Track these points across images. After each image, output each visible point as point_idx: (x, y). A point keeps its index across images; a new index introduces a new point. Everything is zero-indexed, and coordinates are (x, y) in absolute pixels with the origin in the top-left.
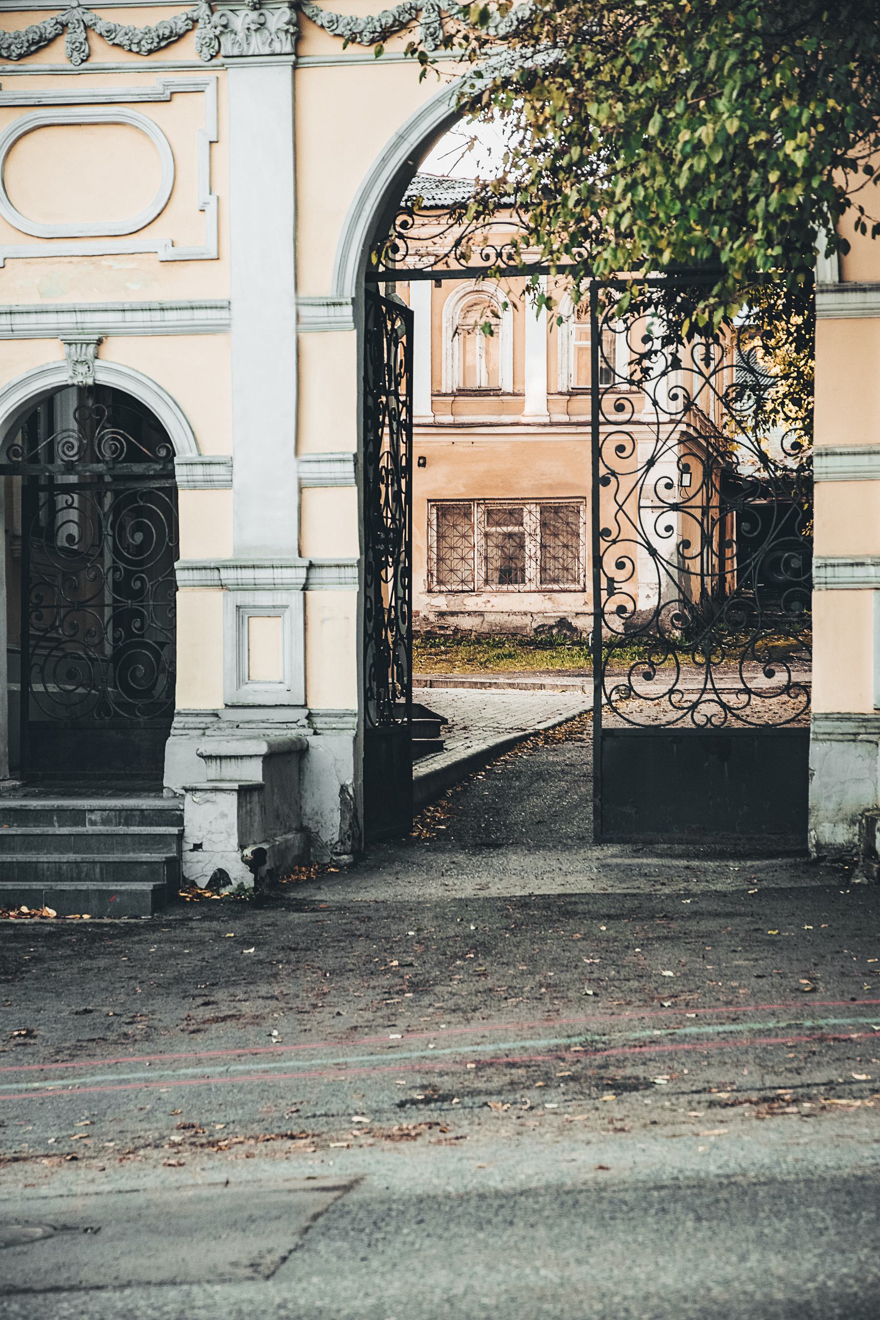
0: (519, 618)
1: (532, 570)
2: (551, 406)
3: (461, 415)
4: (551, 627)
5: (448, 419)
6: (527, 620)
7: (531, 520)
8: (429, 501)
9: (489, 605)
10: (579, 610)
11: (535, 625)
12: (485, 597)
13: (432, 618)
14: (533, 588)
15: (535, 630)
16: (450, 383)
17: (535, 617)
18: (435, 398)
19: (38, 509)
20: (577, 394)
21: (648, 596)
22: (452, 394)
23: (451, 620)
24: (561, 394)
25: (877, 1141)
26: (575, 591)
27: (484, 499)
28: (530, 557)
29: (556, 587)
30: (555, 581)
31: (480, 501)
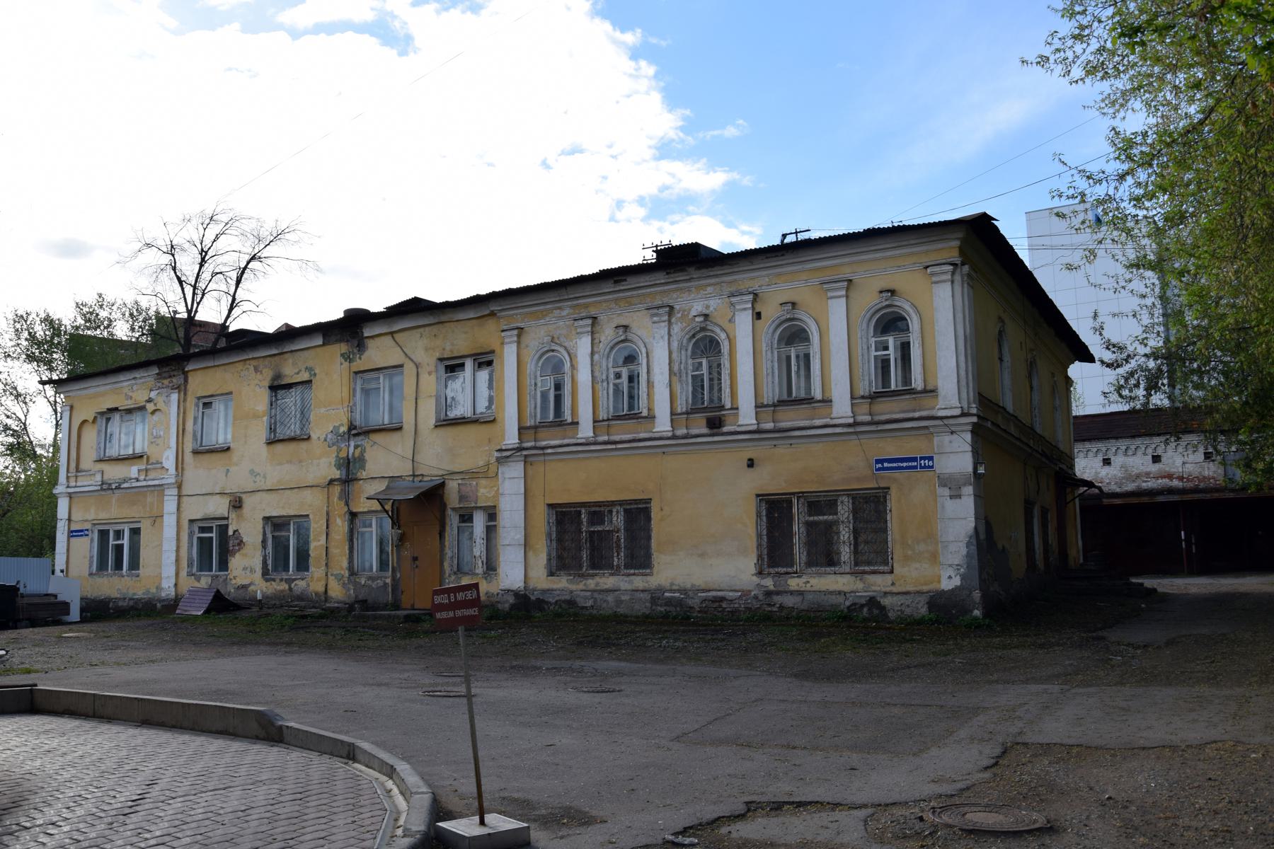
0: (834, 597)
1: (846, 553)
2: (855, 409)
3: (780, 422)
4: (862, 606)
5: (770, 426)
6: (840, 599)
7: (844, 510)
8: (758, 496)
9: (808, 585)
10: (888, 589)
11: (848, 603)
12: (804, 579)
13: (761, 597)
14: (848, 570)
15: (848, 608)
16: (771, 395)
17: (848, 595)
18: (758, 410)
19: (1185, 540)
20: (878, 397)
21: (950, 577)
22: (774, 405)
23: (778, 599)
24: (863, 397)
25: (1273, 844)
26: (883, 573)
27: (803, 493)
28: (844, 542)
29: (867, 568)
30: (869, 563)
31: (800, 495)
